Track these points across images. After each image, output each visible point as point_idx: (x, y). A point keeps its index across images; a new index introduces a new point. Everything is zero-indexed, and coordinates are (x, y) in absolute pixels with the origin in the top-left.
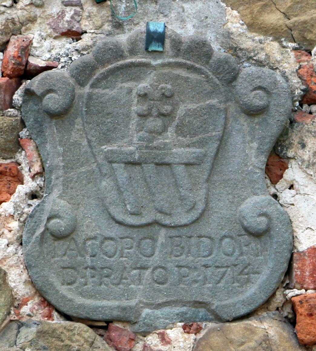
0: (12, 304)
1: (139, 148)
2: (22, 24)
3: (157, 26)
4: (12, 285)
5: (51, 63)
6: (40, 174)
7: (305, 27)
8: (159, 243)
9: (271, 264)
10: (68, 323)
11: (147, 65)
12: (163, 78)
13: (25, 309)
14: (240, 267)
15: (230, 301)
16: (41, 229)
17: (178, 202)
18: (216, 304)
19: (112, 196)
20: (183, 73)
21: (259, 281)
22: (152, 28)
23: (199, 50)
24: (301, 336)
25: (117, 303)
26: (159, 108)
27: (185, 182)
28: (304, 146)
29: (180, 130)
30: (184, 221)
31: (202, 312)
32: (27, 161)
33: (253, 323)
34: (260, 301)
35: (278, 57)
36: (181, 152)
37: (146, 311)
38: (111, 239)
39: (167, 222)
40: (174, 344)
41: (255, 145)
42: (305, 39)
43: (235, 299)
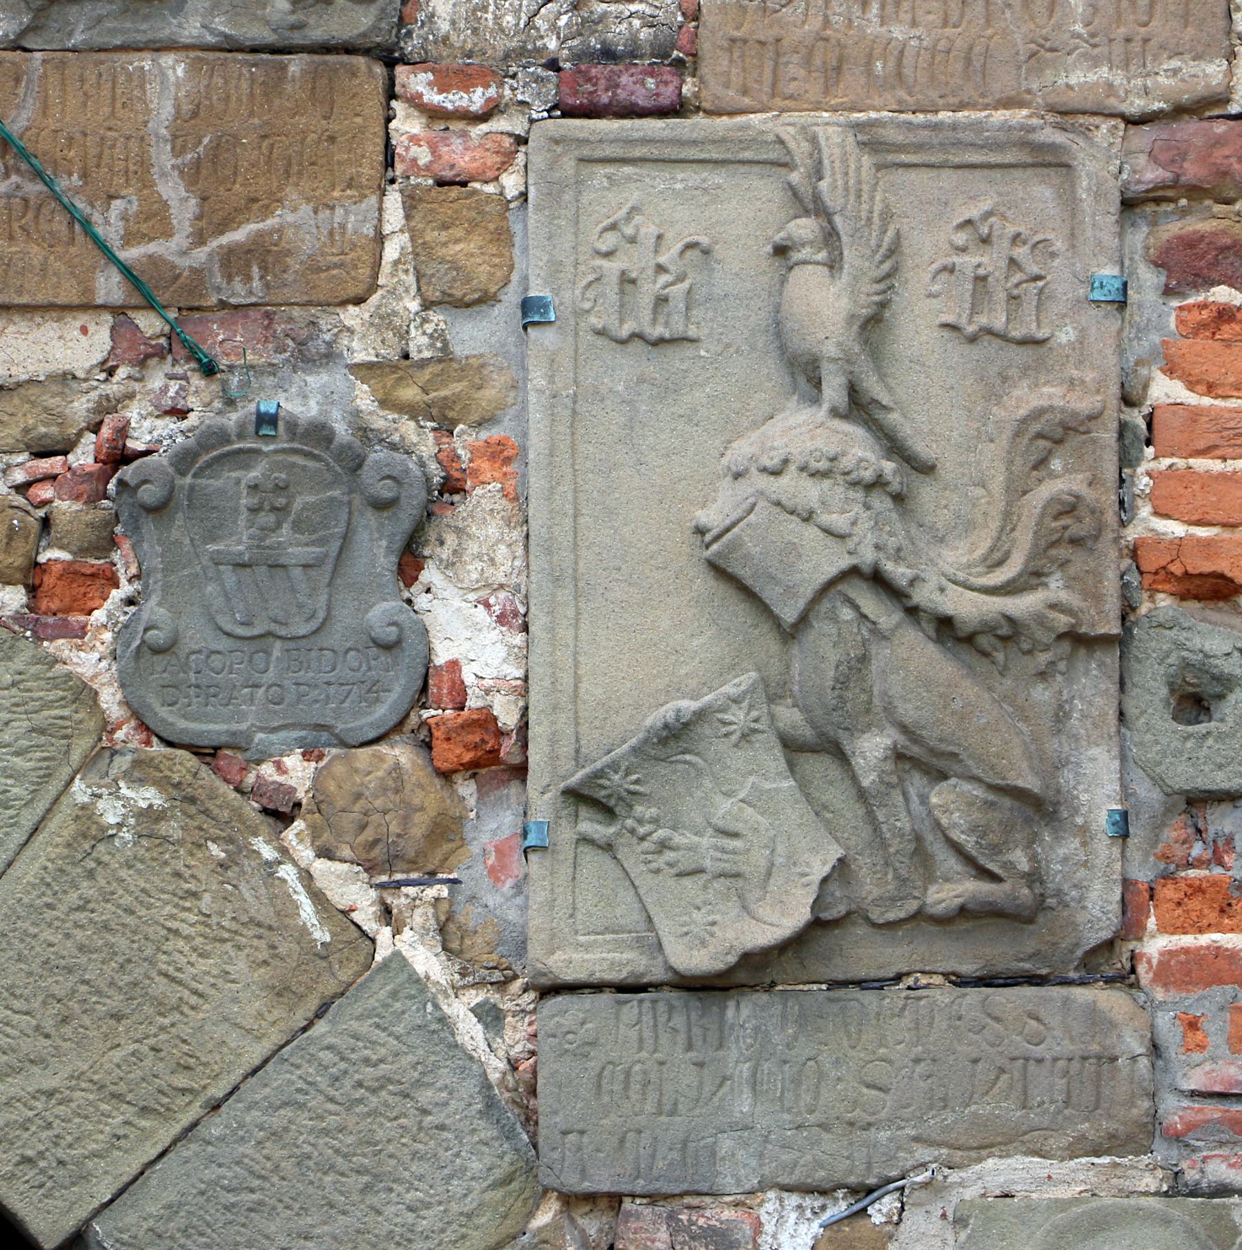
0: (104, 729)
1: (249, 548)
2: (118, 401)
3: (268, 407)
4: (105, 706)
5: (152, 447)
6: (138, 577)
7: (446, 403)
8: (274, 658)
9: (403, 681)
10: (169, 750)
11: (257, 452)
12: (276, 466)
13: (120, 735)
14: (368, 684)
15: (357, 723)
16: (138, 642)
17: (294, 610)
18: (340, 727)
19: (219, 602)
20: (300, 460)
21: (390, 701)
22: (263, 408)
23: (319, 433)
24: (438, 764)
25: (225, 727)
26: (272, 501)
27: (303, 587)
28: (442, 543)
29: (297, 526)
30: (302, 632)
31: (325, 736)
32: (123, 561)
33: (383, 748)
34: (391, 723)
35: (415, 439)
36: (297, 550)
37: (260, 736)
38: (218, 652)
39: (283, 633)
40: (292, 773)
41: (384, 543)
42: (445, 417)
43: (364, 721)
